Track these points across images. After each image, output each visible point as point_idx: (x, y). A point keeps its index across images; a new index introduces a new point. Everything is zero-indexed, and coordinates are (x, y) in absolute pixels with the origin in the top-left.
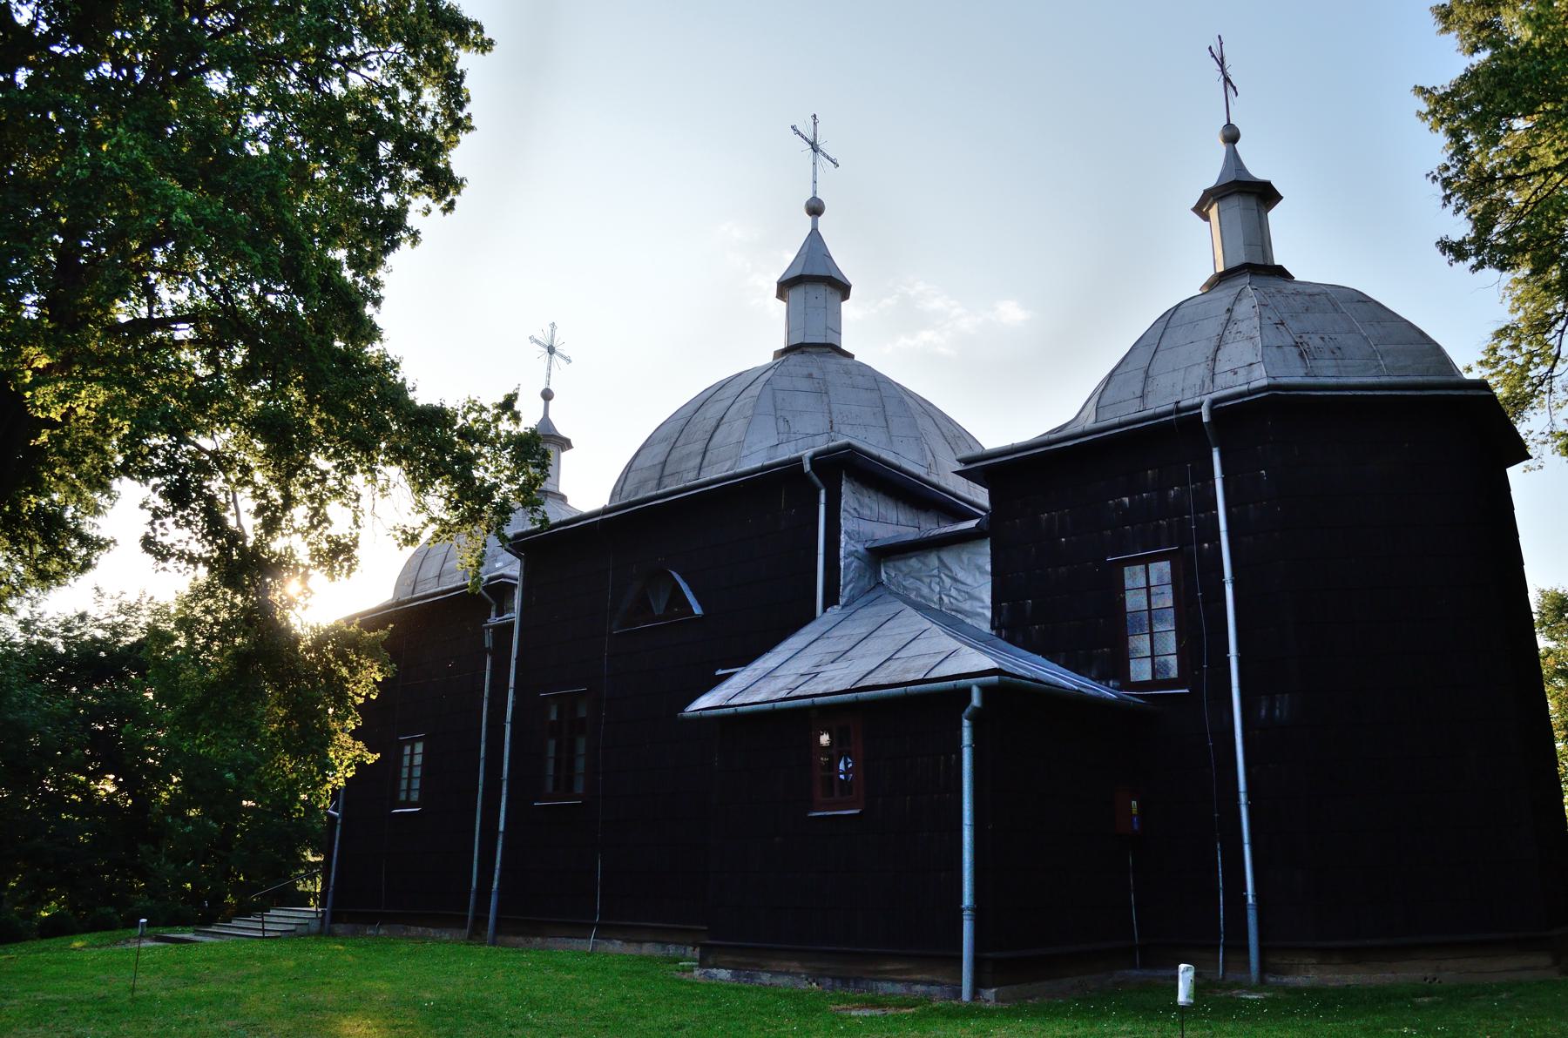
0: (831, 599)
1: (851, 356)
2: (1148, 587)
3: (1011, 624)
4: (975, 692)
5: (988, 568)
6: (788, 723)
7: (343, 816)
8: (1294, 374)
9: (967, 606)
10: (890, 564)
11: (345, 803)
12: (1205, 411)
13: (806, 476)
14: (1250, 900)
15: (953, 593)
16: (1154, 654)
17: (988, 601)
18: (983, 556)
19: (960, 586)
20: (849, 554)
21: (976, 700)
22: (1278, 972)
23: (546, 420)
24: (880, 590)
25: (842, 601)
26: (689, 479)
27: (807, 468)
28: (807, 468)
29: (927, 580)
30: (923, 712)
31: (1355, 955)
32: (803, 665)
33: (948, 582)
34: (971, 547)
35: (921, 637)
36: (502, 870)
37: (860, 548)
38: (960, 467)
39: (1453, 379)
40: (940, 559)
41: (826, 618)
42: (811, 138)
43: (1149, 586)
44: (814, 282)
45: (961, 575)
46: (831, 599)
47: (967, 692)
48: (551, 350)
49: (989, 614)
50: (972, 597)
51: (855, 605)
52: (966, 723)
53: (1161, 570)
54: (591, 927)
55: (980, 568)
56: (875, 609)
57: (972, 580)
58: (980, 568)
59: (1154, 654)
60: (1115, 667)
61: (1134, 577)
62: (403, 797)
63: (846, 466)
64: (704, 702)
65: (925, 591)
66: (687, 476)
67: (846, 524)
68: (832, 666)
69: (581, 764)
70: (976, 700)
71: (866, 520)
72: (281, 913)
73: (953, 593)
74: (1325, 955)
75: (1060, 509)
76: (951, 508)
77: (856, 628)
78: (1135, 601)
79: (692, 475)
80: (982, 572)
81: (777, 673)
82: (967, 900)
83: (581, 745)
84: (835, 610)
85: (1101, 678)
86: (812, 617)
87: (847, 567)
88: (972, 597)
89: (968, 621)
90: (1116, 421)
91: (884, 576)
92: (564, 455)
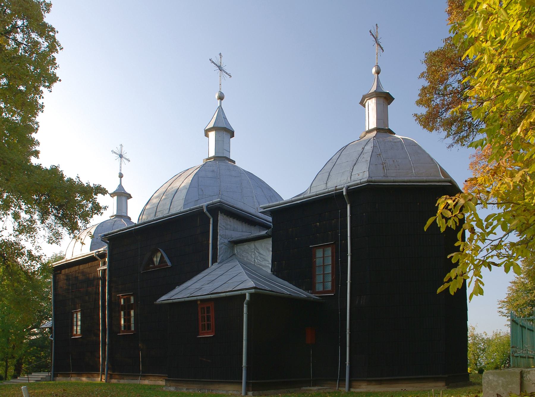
0: (214, 260)
1: (234, 162)
2: (323, 257)
3: (279, 268)
4: (247, 295)
5: (271, 249)
6: (190, 305)
7: (55, 339)
8: (379, 176)
9: (263, 263)
10: (238, 247)
11: (55, 334)
12: (344, 190)
13: (204, 213)
14: (347, 365)
15: (259, 258)
16: (324, 282)
17: (270, 261)
18: (268, 244)
19: (261, 256)
20: (221, 244)
21: (247, 298)
22: (341, 387)
23: (120, 186)
24: (234, 256)
25: (218, 261)
26: (165, 213)
27: (205, 210)
28: (205, 210)
29: (250, 253)
30: (228, 303)
31: (380, 382)
32: (198, 285)
33: (257, 254)
34: (265, 240)
35: (236, 274)
36: (248, 368)
37: (226, 241)
38: (262, 210)
39: (281, 202)
40: (255, 246)
41: (212, 267)
42: (219, 64)
43: (324, 257)
44: (224, 130)
45: (261, 252)
46: (214, 260)
47: (244, 295)
48: (121, 156)
49: (271, 266)
50: (266, 260)
51: (223, 263)
52: (245, 305)
53: (329, 252)
54: (139, 376)
55: (268, 249)
56: (229, 264)
57: (263, 255)
58: (268, 249)
59: (324, 282)
60: (310, 286)
61: (319, 253)
62: (75, 333)
63: (219, 209)
64: (164, 298)
65: (249, 257)
66: (164, 213)
67: (220, 232)
68: (208, 285)
69: (132, 319)
70: (247, 298)
71: (228, 229)
72: (36, 374)
73: (259, 258)
74: (369, 382)
75: (298, 226)
76: (263, 226)
77: (219, 272)
78: (319, 261)
79: (167, 211)
80: (269, 251)
81: (189, 288)
82: (244, 364)
83: (132, 313)
84: (216, 265)
85: (306, 290)
86: (208, 267)
87: (221, 248)
88: (266, 260)
89: (264, 269)
90: (315, 193)
91: (236, 252)
92: (129, 201)
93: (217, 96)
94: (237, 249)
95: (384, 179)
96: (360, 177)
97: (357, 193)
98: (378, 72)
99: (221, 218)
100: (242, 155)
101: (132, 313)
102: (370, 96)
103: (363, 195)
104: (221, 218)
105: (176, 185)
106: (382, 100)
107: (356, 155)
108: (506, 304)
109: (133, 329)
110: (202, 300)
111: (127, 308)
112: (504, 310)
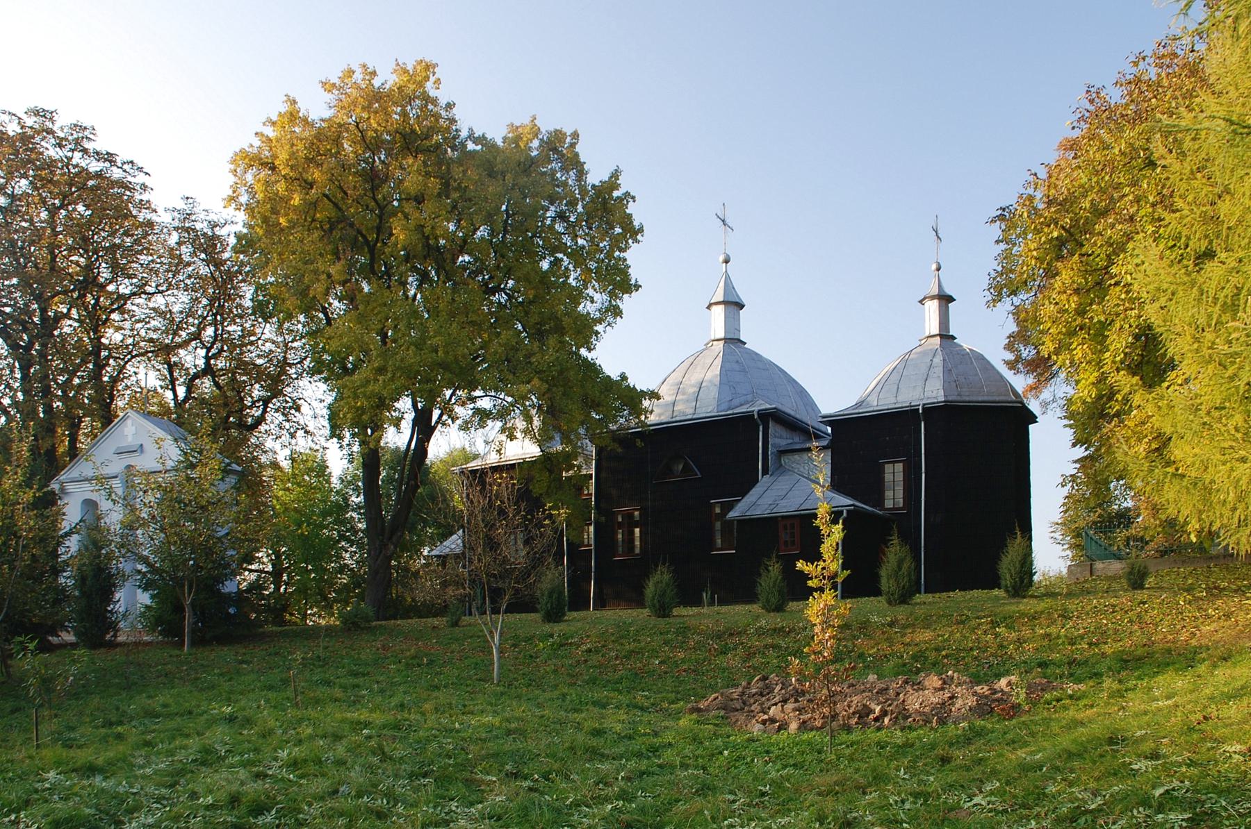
0: (765, 472)
16: (894, 497)
41: (764, 481)
43: (894, 473)
53: (899, 467)
59: (894, 497)
61: (888, 468)
75: (861, 442)
78: (888, 477)
86: (757, 481)
93: (722, 258)
94: (785, 460)
95: (959, 398)
96: (934, 395)
97: (932, 412)
98: (938, 269)
99: (773, 428)
100: (755, 337)
101: (637, 530)
102: (933, 298)
103: (944, 417)
104: (773, 428)
105: (695, 377)
106: (944, 302)
107: (924, 369)
108: (1060, 527)
109: (637, 551)
110: (783, 517)
111: (630, 524)
112: (1058, 535)
